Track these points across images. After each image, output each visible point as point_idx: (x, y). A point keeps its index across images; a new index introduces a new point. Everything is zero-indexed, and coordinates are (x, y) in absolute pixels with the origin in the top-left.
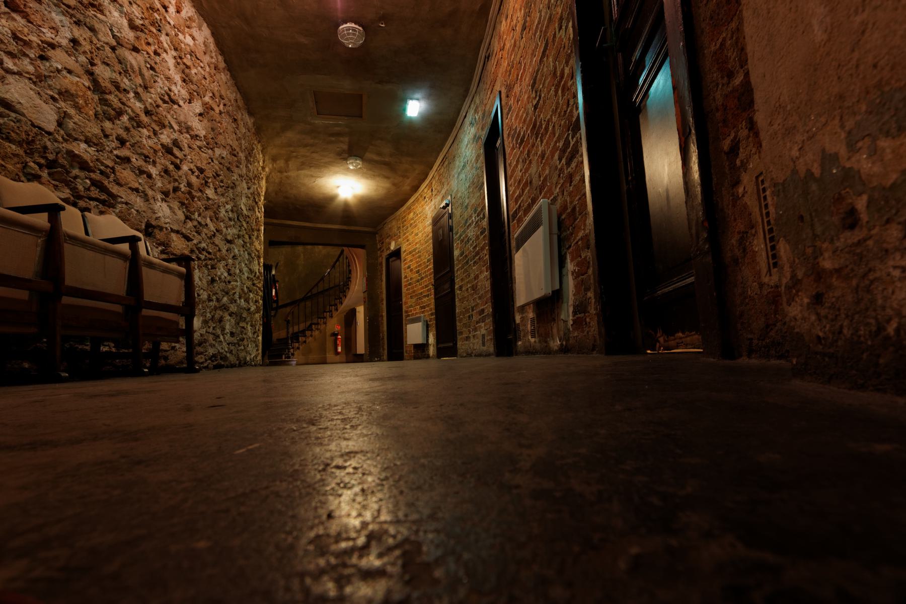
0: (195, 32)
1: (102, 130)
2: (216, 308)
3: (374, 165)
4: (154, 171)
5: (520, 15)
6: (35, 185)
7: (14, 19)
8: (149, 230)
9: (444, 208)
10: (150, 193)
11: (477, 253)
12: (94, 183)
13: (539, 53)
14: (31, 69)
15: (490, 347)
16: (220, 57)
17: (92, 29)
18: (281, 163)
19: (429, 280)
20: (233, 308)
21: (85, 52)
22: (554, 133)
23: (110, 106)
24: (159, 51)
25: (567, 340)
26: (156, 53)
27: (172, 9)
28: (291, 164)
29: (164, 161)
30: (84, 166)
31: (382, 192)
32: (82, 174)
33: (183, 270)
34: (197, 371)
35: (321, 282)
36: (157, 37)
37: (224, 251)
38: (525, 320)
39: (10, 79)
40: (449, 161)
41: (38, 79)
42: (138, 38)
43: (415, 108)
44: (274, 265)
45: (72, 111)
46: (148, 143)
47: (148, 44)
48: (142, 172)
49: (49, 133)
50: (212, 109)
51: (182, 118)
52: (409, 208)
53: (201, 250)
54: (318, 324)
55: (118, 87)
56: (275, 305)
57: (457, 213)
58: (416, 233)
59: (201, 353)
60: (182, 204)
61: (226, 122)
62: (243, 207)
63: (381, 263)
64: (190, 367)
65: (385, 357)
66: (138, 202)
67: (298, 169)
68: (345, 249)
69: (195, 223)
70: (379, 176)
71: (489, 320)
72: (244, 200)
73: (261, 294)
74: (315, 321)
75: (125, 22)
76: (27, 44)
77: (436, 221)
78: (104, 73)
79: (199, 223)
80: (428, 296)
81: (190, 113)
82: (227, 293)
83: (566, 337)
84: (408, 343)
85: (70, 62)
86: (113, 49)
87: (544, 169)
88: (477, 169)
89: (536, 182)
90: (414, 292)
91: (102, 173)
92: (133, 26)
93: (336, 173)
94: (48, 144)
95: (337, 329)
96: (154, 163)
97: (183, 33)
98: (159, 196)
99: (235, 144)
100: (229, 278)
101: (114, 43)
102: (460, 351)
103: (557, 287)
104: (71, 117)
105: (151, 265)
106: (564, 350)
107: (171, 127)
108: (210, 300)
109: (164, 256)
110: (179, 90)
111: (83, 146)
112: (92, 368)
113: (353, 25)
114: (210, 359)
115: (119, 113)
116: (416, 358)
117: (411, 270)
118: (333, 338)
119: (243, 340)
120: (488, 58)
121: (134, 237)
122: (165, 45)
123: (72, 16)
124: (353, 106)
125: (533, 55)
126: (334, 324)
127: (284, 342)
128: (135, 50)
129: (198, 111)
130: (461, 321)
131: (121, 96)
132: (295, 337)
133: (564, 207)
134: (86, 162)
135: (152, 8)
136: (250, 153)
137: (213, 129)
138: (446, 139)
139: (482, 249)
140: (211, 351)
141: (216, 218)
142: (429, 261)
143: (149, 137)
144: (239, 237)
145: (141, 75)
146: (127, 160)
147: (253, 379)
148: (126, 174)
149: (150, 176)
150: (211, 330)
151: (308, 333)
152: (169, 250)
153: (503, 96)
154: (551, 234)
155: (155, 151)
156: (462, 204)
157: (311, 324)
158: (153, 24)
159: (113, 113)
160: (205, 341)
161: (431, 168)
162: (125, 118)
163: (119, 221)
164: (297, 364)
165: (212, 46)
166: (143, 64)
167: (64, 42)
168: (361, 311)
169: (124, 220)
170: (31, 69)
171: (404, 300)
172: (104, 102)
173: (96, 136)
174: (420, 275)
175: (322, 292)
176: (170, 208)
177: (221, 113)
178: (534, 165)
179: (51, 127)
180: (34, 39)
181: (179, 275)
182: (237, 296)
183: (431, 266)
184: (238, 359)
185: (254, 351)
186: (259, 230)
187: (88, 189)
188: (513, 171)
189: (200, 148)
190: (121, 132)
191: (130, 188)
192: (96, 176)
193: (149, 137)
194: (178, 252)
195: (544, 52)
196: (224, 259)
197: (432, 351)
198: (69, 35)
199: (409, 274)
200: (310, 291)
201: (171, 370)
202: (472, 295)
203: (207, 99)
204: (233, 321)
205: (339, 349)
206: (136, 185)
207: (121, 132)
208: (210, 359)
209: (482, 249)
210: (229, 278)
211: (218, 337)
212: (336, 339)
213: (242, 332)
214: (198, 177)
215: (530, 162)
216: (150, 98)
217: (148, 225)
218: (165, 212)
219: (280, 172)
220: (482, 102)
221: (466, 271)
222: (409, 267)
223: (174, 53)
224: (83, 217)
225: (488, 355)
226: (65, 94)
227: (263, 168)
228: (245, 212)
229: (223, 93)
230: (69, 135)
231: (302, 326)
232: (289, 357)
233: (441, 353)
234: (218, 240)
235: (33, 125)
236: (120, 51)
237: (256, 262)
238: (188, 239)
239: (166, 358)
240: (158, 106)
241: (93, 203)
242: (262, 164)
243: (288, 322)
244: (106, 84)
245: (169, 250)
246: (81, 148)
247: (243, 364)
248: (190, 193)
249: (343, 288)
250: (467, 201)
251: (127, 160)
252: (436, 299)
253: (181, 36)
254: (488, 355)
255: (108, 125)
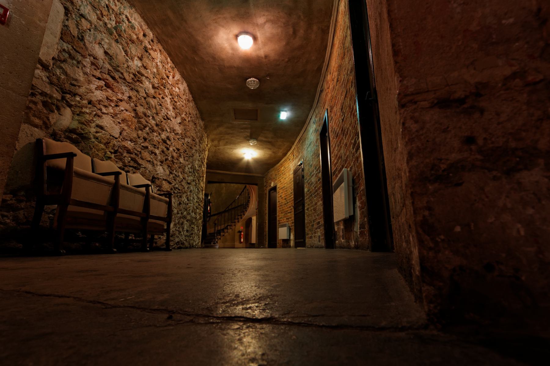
0: (180, 86)
1: (138, 135)
2: (180, 218)
3: (262, 143)
4: (157, 152)
5: (336, 74)
6: (109, 162)
7: (108, 91)
8: (153, 180)
9: (300, 165)
10: (155, 162)
11: (316, 191)
12: (132, 159)
13: (344, 94)
14: (112, 111)
15: (323, 243)
16: (190, 96)
17: (137, 91)
18: (216, 143)
19: (291, 204)
20: (189, 217)
21: (133, 102)
22: (350, 135)
23: (141, 124)
24: (164, 97)
25: (358, 242)
26: (163, 98)
27: (171, 77)
28: (221, 143)
29: (162, 147)
30: (129, 152)
31: (267, 156)
32: (127, 155)
33: (168, 199)
34: (171, 250)
35: (234, 205)
36: (163, 91)
37: (186, 188)
38: (339, 229)
39: (104, 116)
40: (303, 140)
41: (114, 116)
42: (155, 92)
43: (284, 115)
44: (210, 193)
45: (126, 128)
46: (156, 139)
47: (160, 94)
48: (152, 153)
49: (116, 138)
50: (185, 120)
51: (171, 126)
52: (282, 164)
53: (175, 188)
54: (231, 226)
55: (145, 115)
56: (209, 215)
57: (306, 169)
58: (285, 178)
59: (172, 241)
60: (169, 166)
61: (191, 125)
62: (196, 166)
63: (266, 194)
64: (167, 248)
65: (267, 246)
66: (150, 166)
67: (225, 145)
68: (247, 185)
69: (174, 175)
70: (266, 148)
71: (322, 228)
72: (197, 162)
73: (202, 209)
74: (230, 224)
75: (151, 86)
76: (111, 101)
77: (295, 172)
78: (140, 109)
79: (176, 175)
80: (290, 212)
81: (175, 123)
82: (186, 210)
83: (356, 241)
84: (280, 238)
85: (127, 106)
86: (145, 98)
87: (346, 152)
88: (317, 146)
89: (344, 158)
90: (283, 210)
91: (136, 154)
92: (154, 87)
93: (244, 147)
94: (116, 143)
95: (241, 229)
96: (158, 148)
97: (175, 87)
98: (159, 163)
99: (194, 135)
100: (187, 202)
101: (145, 96)
102: (307, 245)
103: (352, 214)
104: (125, 130)
105: (154, 198)
106: (357, 247)
107: (167, 131)
108: (178, 213)
109: (159, 192)
110: (171, 113)
111: (129, 142)
112: (125, 247)
113: (254, 79)
114: (176, 244)
115: (145, 127)
116: (283, 247)
117: (282, 198)
118: (239, 234)
119: (192, 234)
120: (322, 91)
121: (148, 185)
122: (167, 94)
123: (130, 86)
124: (252, 115)
125: (342, 95)
126: (240, 226)
127: (213, 236)
128: (154, 98)
129: (179, 122)
130: (308, 227)
131: (146, 119)
132: (219, 232)
133: (355, 173)
134: (130, 150)
135: (162, 78)
136: (201, 139)
137: (185, 129)
138: (301, 130)
139: (319, 189)
140: (177, 240)
141: (183, 172)
142: (291, 193)
143: (157, 136)
144: (193, 181)
145: (156, 108)
146: (147, 147)
147: (195, 256)
148: (146, 154)
149: (156, 154)
150: (177, 229)
151: (226, 230)
152: (162, 189)
153: (329, 111)
154: (348, 186)
155: (159, 143)
156: (309, 164)
157: (227, 226)
158: (162, 85)
159: (142, 127)
160: (174, 234)
161: (293, 144)
162: (147, 129)
163: (141, 176)
164: (219, 248)
165: (187, 91)
166: (157, 103)
167: (126, 98)
168: (254, 219)
169: (143, 175)
170: (112, 111)
171: (278, 214)
172: (139, 122)
173: (135, 138)
174: (286, 201)
175: (234, 208)
176: (163, 169)
177: (189, 121)
178: (342, 148)
179: (117, 136)
180: (114, 98)
181: (166, 202)
182: (191, 211)
183: (293, 196)
184: (189, 244)
185: (197, 240)
186: (203, 177)
187: (129, 162)
188: (334, 150)
189: (178, 139)
190: (145, 135)
191: (148, 161)
192: (133, 156)
193: (157, 136)
194: (165, 190)
195: (346, 95)
196: (186, 193)
197: (292, 243)
198: (128, 95)
199: (281, 200)
200: (228, 207)
201: (158, 249)
202: (314, 213)
203: (183, 116)
204: (188, 224)
205: (242, 240)
206: (149, 159)
207: (145, 135)
208: (176, 244)
209: (319, 189)
210: (187, 202)
211: (181, 232)
212: (241, 234)
213: (192, 230)
214: (176, 153)
215: (341, 147)
216: (159, 118)
217: (153, 177)
218: (161, 171)
219: (215, 146)
220: (319, 112)
221: (311, 200)
222: (281, 196)
223: (170, 97)
224: (127, 175)
225: (322, 247)
226: (124, 120)
227: (207, 145)
228: (197, 168)
229: (191, 112)
230: (124, 138)
231: (223, 227)
232: (215, 244)
233: (297, 245)
234: (184, 183)
235: (111, 136)
236: (148, 99)
237: (201, 193)
238: (170, 183)
239: (156, 243)
240: (162, 122)
241: (131, 168)
242: (207, 144)
243: (215, 224)
244: (141, 114)
245: (162, 189)
246: (129, 144)
247: (191, 247)
248: (172, 161)
249: (245, 206)
250: (311, 162)
251: (147, 147)
252: (295, 215)
253: (174, 89)
254: (322, 247)
255: (140, 132)
